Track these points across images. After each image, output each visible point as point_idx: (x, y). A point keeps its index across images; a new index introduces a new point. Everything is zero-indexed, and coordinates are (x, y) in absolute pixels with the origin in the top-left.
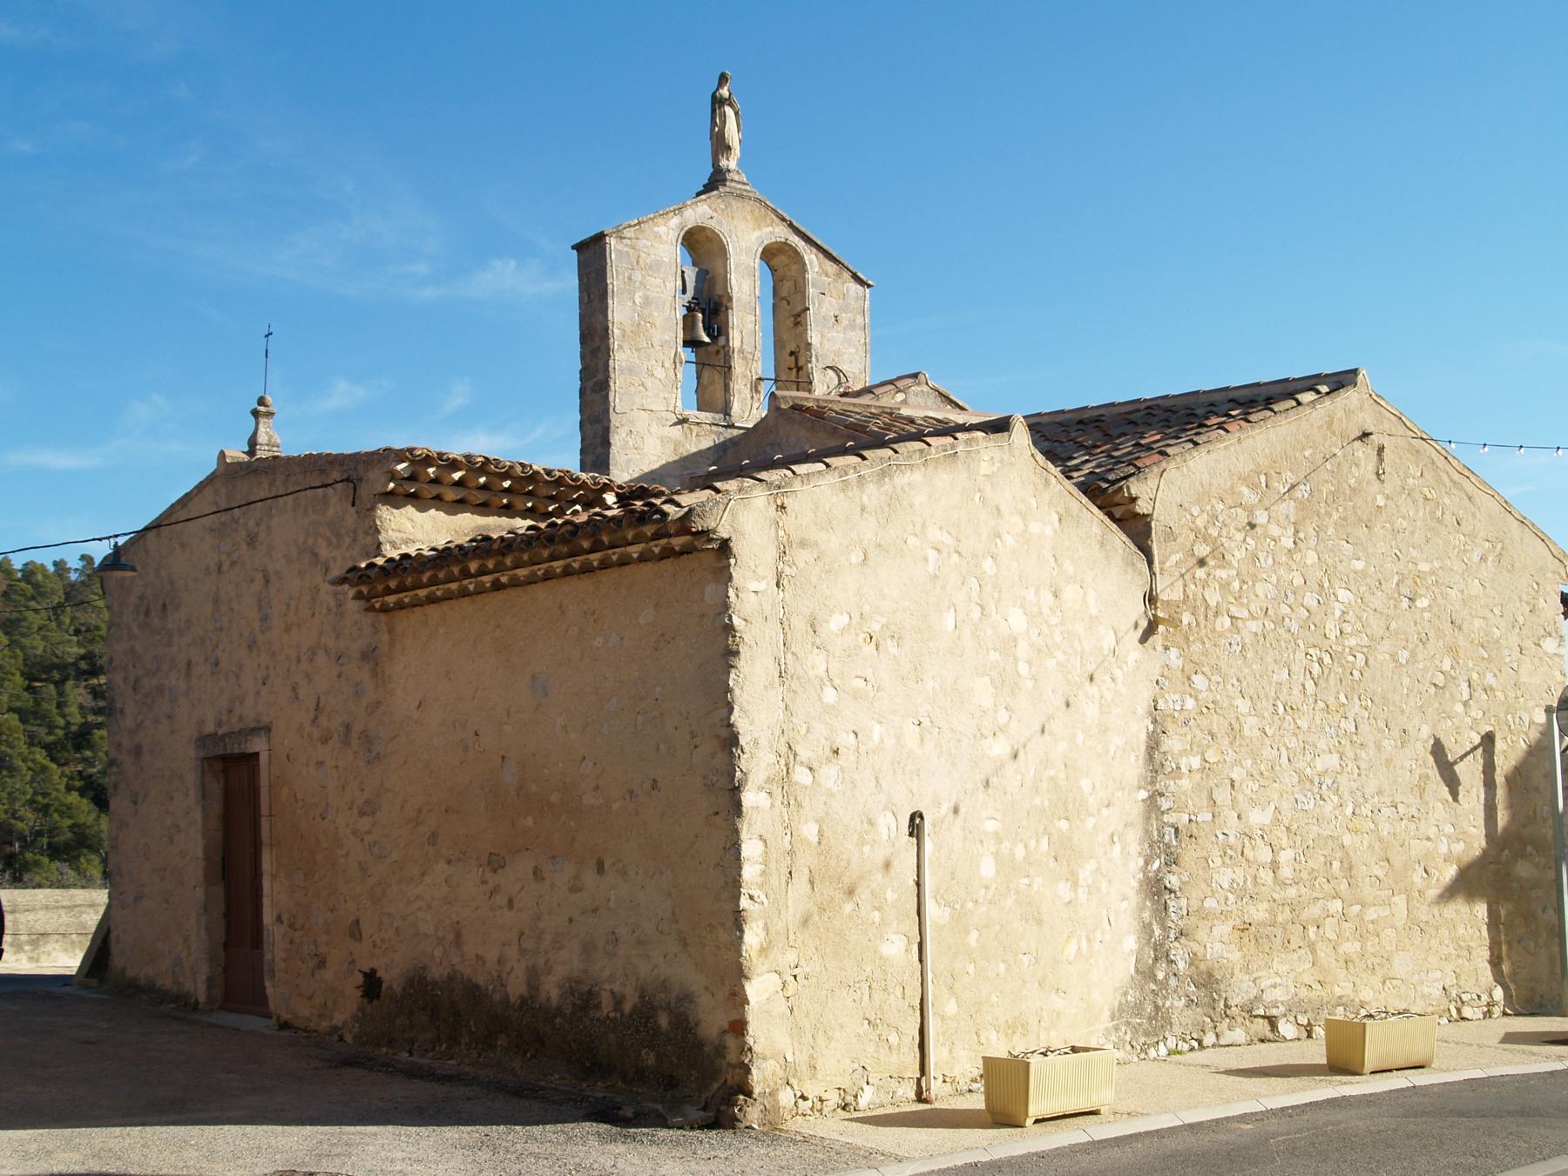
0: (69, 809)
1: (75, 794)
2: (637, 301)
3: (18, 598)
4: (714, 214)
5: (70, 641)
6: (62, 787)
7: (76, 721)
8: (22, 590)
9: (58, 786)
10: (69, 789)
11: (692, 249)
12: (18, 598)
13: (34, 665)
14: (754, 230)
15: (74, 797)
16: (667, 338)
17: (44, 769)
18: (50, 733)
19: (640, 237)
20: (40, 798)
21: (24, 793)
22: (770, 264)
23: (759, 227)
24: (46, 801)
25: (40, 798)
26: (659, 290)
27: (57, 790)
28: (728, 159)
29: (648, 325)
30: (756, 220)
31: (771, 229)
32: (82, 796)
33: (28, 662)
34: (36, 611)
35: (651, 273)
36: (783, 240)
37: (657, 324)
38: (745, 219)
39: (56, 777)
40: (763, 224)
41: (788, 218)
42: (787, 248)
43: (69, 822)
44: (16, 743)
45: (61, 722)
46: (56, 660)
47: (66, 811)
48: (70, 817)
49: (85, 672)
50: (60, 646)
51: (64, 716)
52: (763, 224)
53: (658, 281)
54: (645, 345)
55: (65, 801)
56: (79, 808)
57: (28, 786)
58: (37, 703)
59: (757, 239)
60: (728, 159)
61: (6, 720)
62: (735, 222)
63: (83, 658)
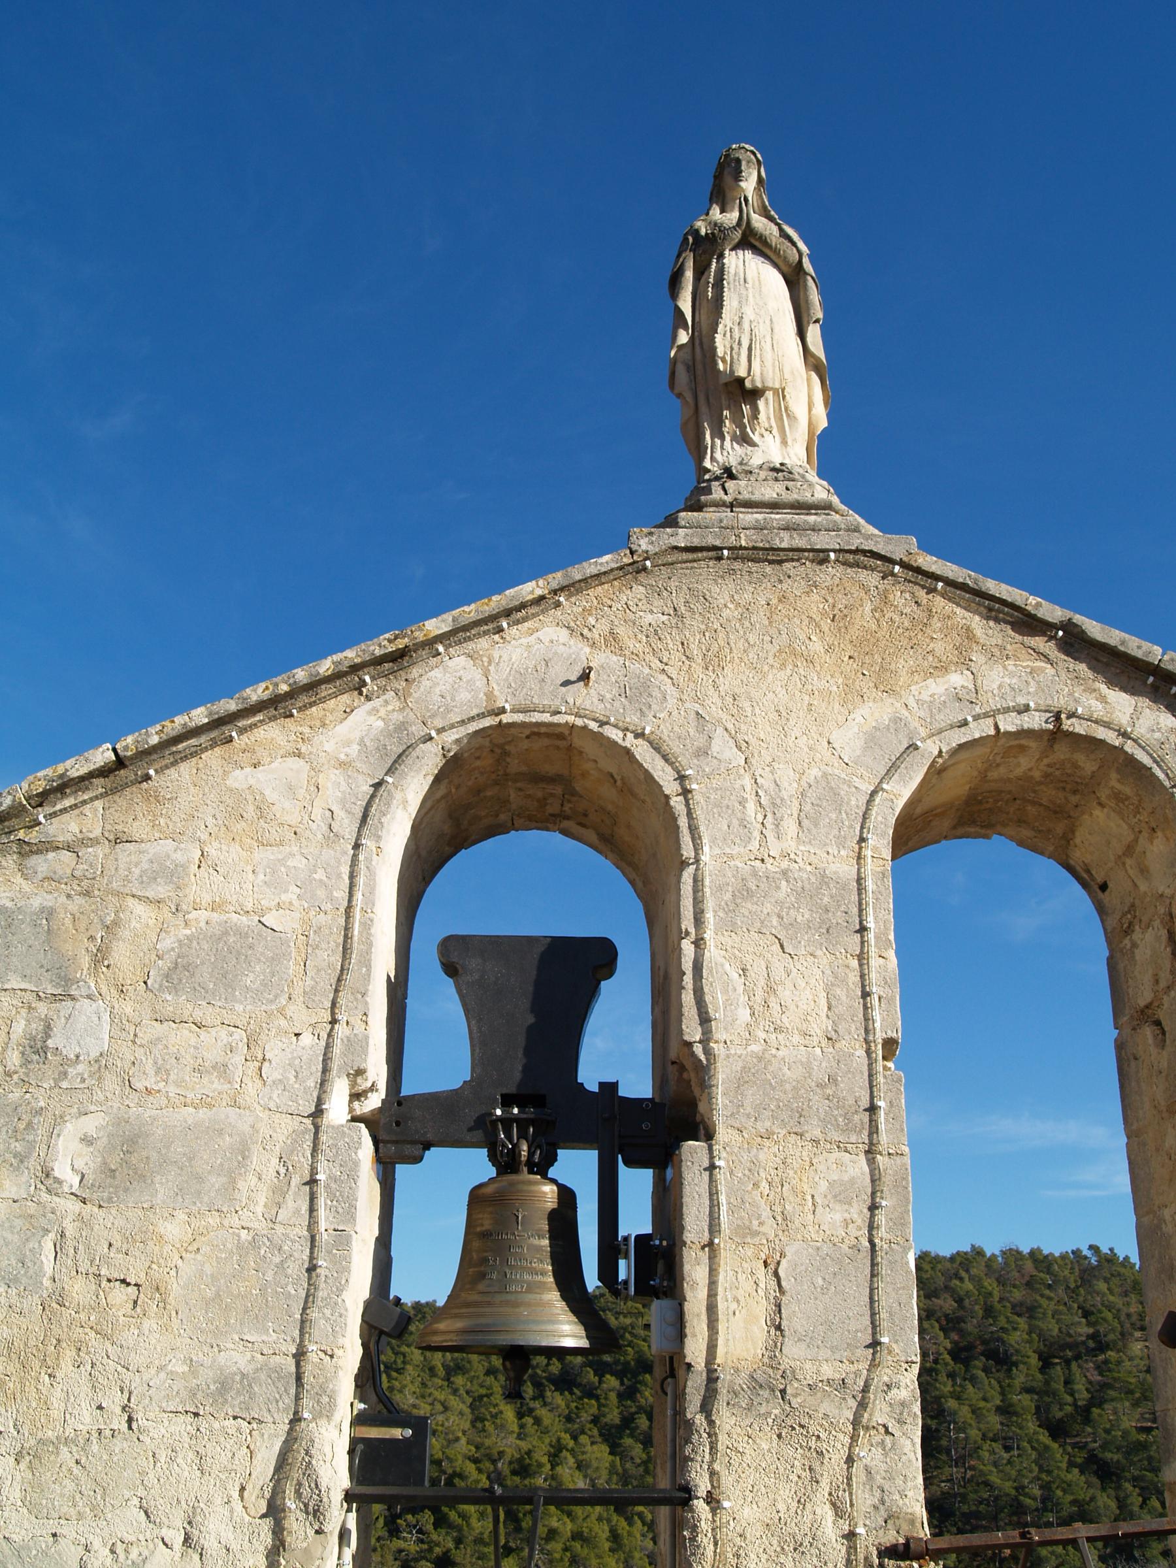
0: (1069, 1485)
1: (1076, 1471)
2: (63, 1170)
3: (1038, 1286)
4: (600, 659)
5: (1080, 1323)
6: (1064, 1465)
7: (1082, 1396)
8: (1042, 1279)
9: (1060, 1464)
10: (1071, 1464)
11: (630, 864)
12: (1038, 1286)
13: (1052, 1344)
14: (851, 696)
15: (1074, 1475)
16: (237, 1359)
17: (1047, 1448)
18: (1061, 1410)
19: (139, 829)
20: (1044, 1476)
21: (1031, 1471)
22: (1078, 856)
23: (885, 683)
24: (1049, 1479)
25: (1044, 1476)
26: (213, 1085)
27: (1059, 1468)
28: (744, 439)
29: (120, 1296)
30: (864, 647)
31: (958, 679)
32: (1082, 1472)
33: (1047, 1343)
34: (1049, 1299)
35: (171, 1002)
36: (1036, 721)
37: (175, 1289)
38: (791, 654)
39: (1058, 1456)
40: (904, 664)
41: (1053, 613)
42: (1088, 765)
43: (1069, 1498)
44: (1024, 1423)
45: (1069, 1399)
46: (1068, 1340)
47: (1067, 1487)
48: (1072, 1494)
49: (1093, 1350)
50: (1073, 1327)
51: (1072, 1395)
52: (904, 664)
53: (213, 1043)
54: (86, 1419)
55: (1065, 1479)
56: (1077, 1485)
57: (1033, 1465)
58: (1047, 1383)
59: (872, 740)
60: (744, 439)
61: (1020, 1400)
62: (729, 680)
63: (1089, 1337)
